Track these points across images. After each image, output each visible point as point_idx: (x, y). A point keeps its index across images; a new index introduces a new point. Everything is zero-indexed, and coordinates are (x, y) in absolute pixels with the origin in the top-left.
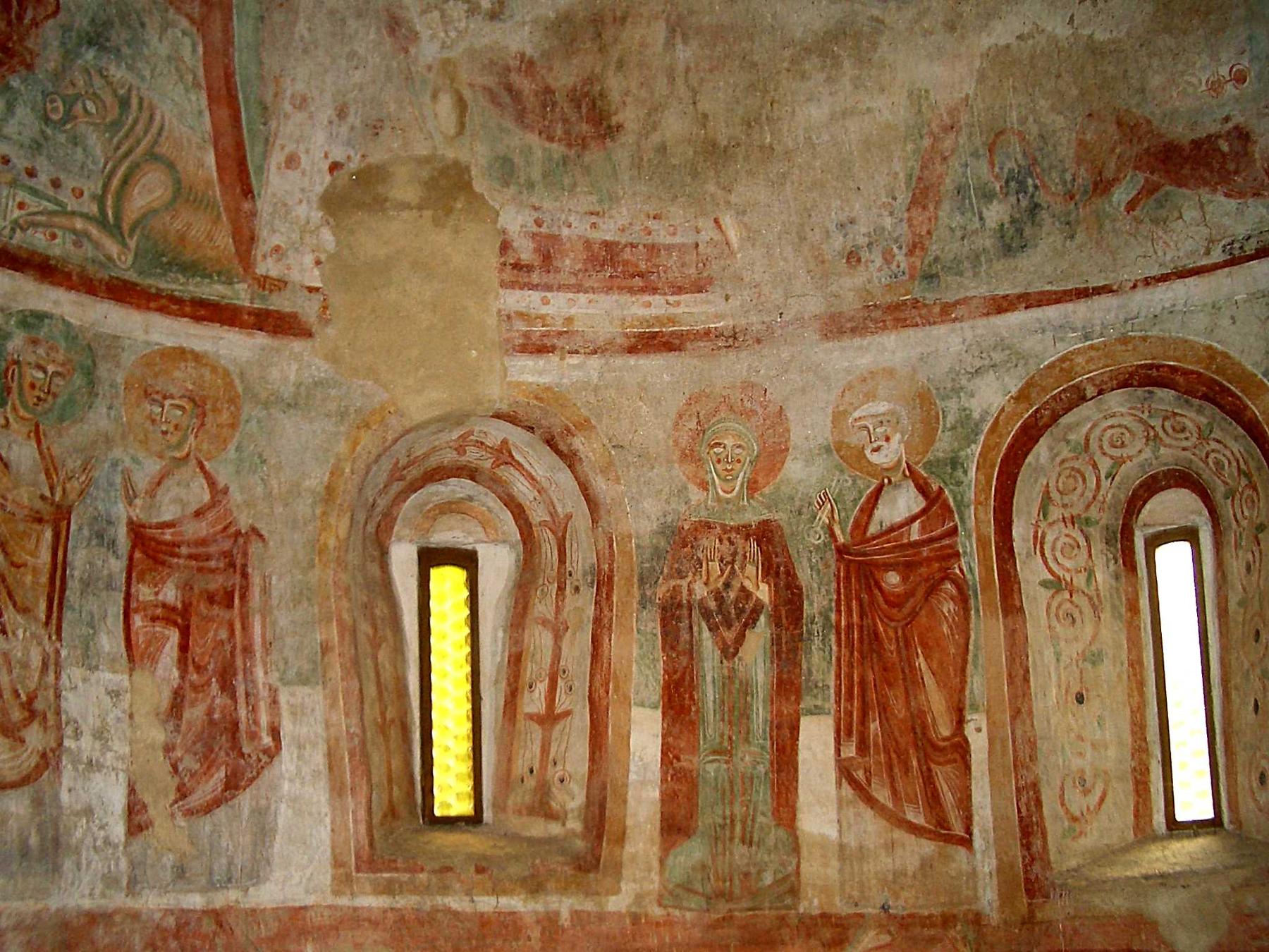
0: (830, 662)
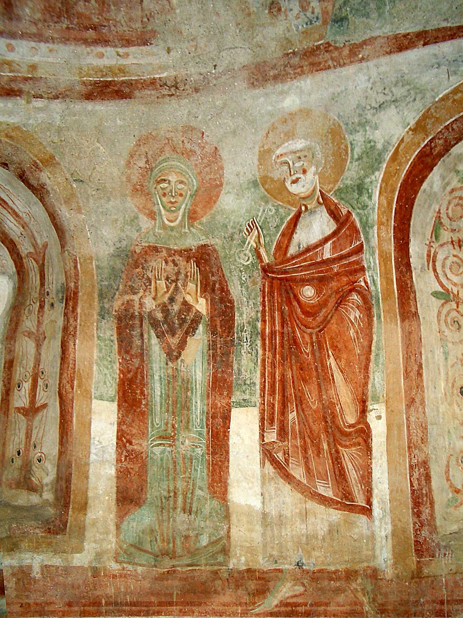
0: (256, 364)
